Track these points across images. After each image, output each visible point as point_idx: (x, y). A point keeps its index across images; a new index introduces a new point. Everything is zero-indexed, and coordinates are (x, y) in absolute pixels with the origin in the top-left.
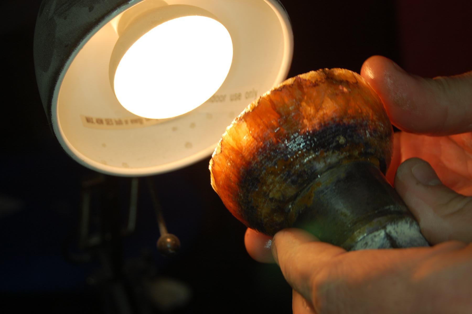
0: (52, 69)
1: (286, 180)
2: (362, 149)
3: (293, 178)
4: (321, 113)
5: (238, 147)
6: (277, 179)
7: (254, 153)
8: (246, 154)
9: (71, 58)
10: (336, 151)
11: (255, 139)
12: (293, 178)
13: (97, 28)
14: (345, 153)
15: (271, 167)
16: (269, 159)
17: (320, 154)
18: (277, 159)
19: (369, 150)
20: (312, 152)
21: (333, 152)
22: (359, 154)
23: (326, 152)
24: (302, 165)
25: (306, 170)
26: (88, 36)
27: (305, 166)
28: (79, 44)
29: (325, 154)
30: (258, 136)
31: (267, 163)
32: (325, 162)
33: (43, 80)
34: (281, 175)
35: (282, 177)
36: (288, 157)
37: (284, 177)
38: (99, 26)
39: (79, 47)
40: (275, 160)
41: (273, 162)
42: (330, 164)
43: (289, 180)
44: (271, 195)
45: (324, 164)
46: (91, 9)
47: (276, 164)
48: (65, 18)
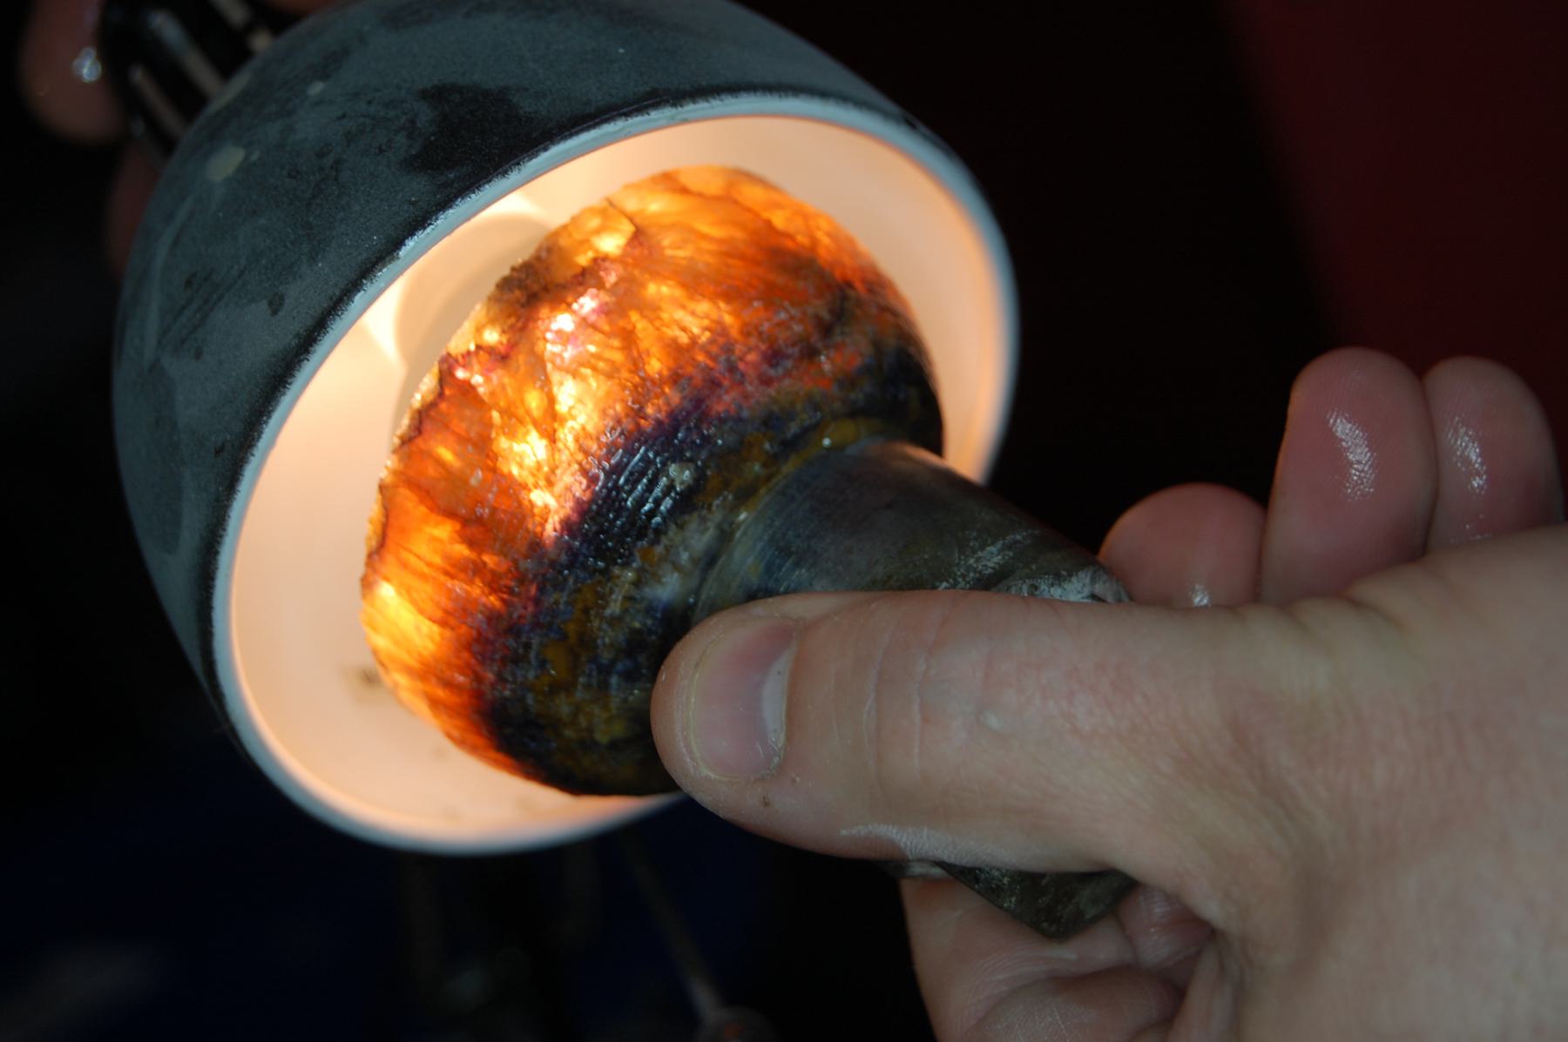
0: (189, 539)
1: (604, 686)
2: (767, 446)
3: (620, 666)
4: (566, 435)
5: (730, 293)
6: (579, 695)
7: (468, 665)
8: (455, 661)
9: (243, 487)
10: (686, 517)
11: (443, 623)
12: (620, 666)
13: (307, 367)
14: (717, 502)
15: (537, 677)
16: (516, 660)
17: (644, 558)
18: (535, 647)
19: (793, 428)
20: (616, 571)
21: (681, 527)
22: (764, 465)
23: (656, 541)
24: (614, 621)
25: (637, 625)
26: (285, 401)
27: (628, 619)
28: (260, 433)
29: (659, 549)
30: (446, 612)
31: (519, 673)
32: (677, 567)
33: (170, 575)
34: (582, 680)
35: (588, 686)
36: (603, 560)
37: (594, 682)
38: (314, 359)
39: (261, 444)
40: (532, 655)
41: (534, 662)
42: (694, 561)
43: (614, 680)
44: (602, 737)
45: (676, 575)
46: (276, 305)
47: (543, 664)
48: (198, 355)
